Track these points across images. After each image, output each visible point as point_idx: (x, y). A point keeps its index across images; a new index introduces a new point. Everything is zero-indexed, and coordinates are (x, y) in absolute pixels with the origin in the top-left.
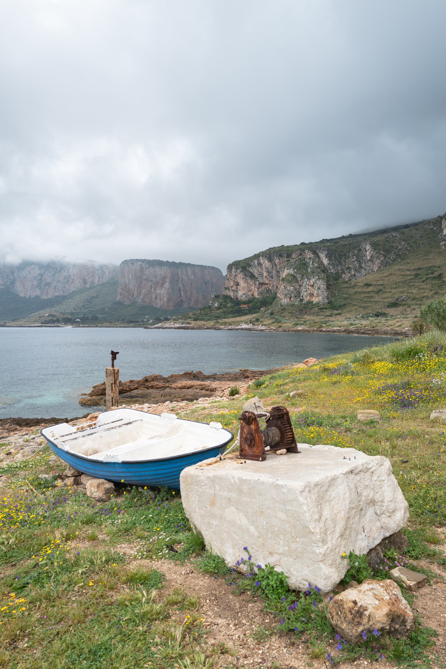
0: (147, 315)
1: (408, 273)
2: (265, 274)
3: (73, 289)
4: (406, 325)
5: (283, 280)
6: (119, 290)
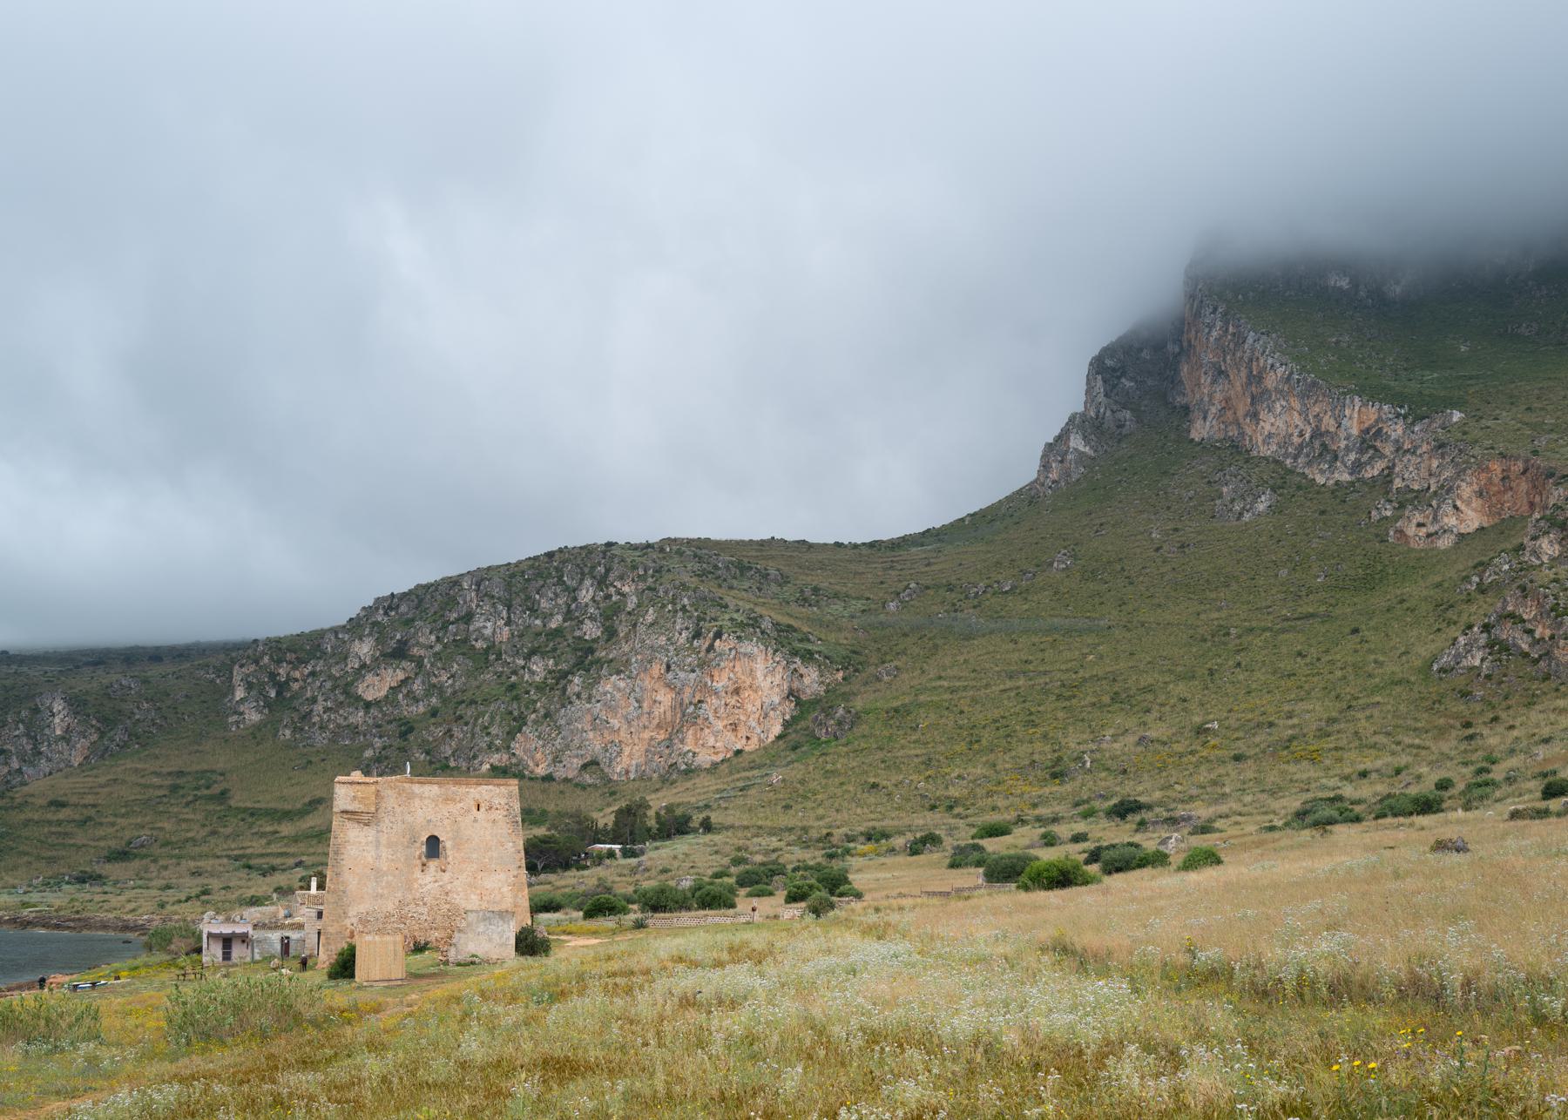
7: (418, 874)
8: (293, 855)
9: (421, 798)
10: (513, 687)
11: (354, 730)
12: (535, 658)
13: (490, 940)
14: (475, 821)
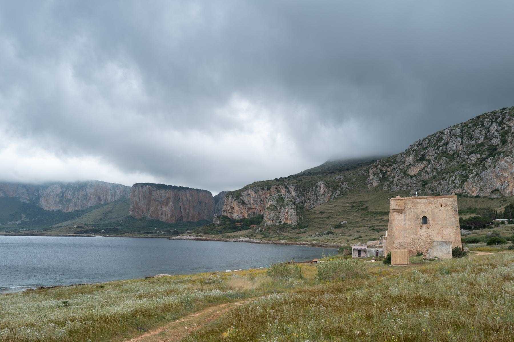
0: (155, 227)
1: (347, 205)
2: (252, 202)
3: (89, 205)
5: (268, 208)
6: (131, 207)
7: (419, 229)
9: (420, 204)
10: (463, 166)
11: (408, 185)
12: (472, 155)
13: (442, 252)
14: (440, 210)
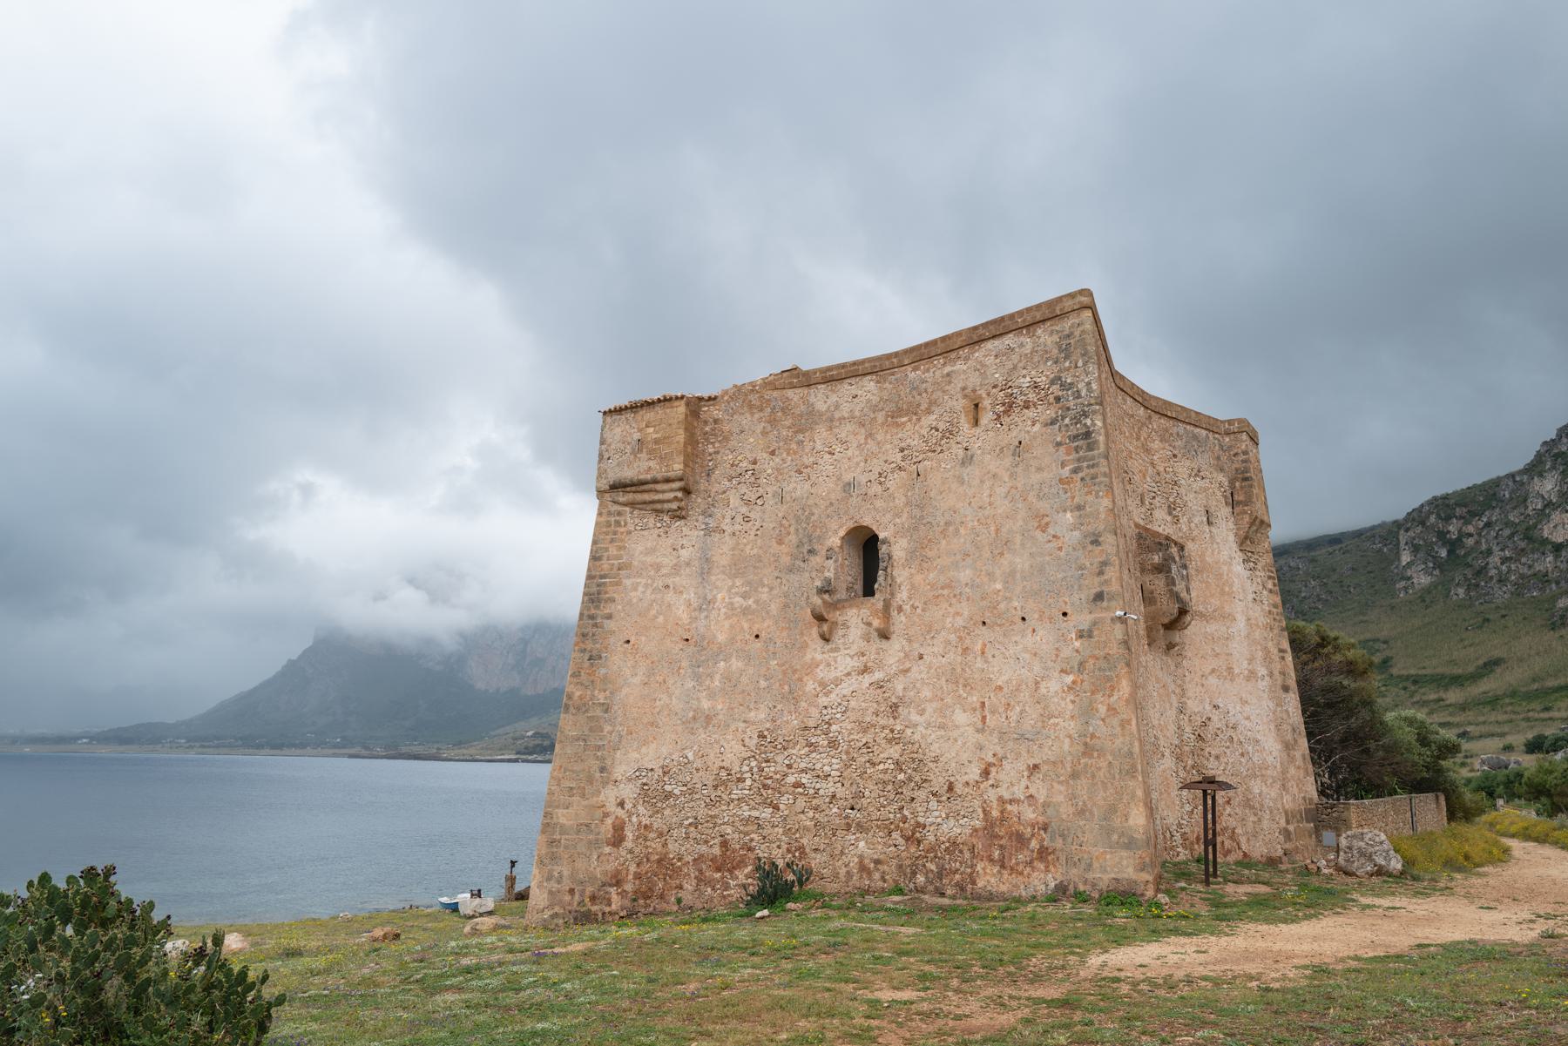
4: (1539, 708)
7: (816, 651)
8: (1458, 725)
11: (1544, 578)
